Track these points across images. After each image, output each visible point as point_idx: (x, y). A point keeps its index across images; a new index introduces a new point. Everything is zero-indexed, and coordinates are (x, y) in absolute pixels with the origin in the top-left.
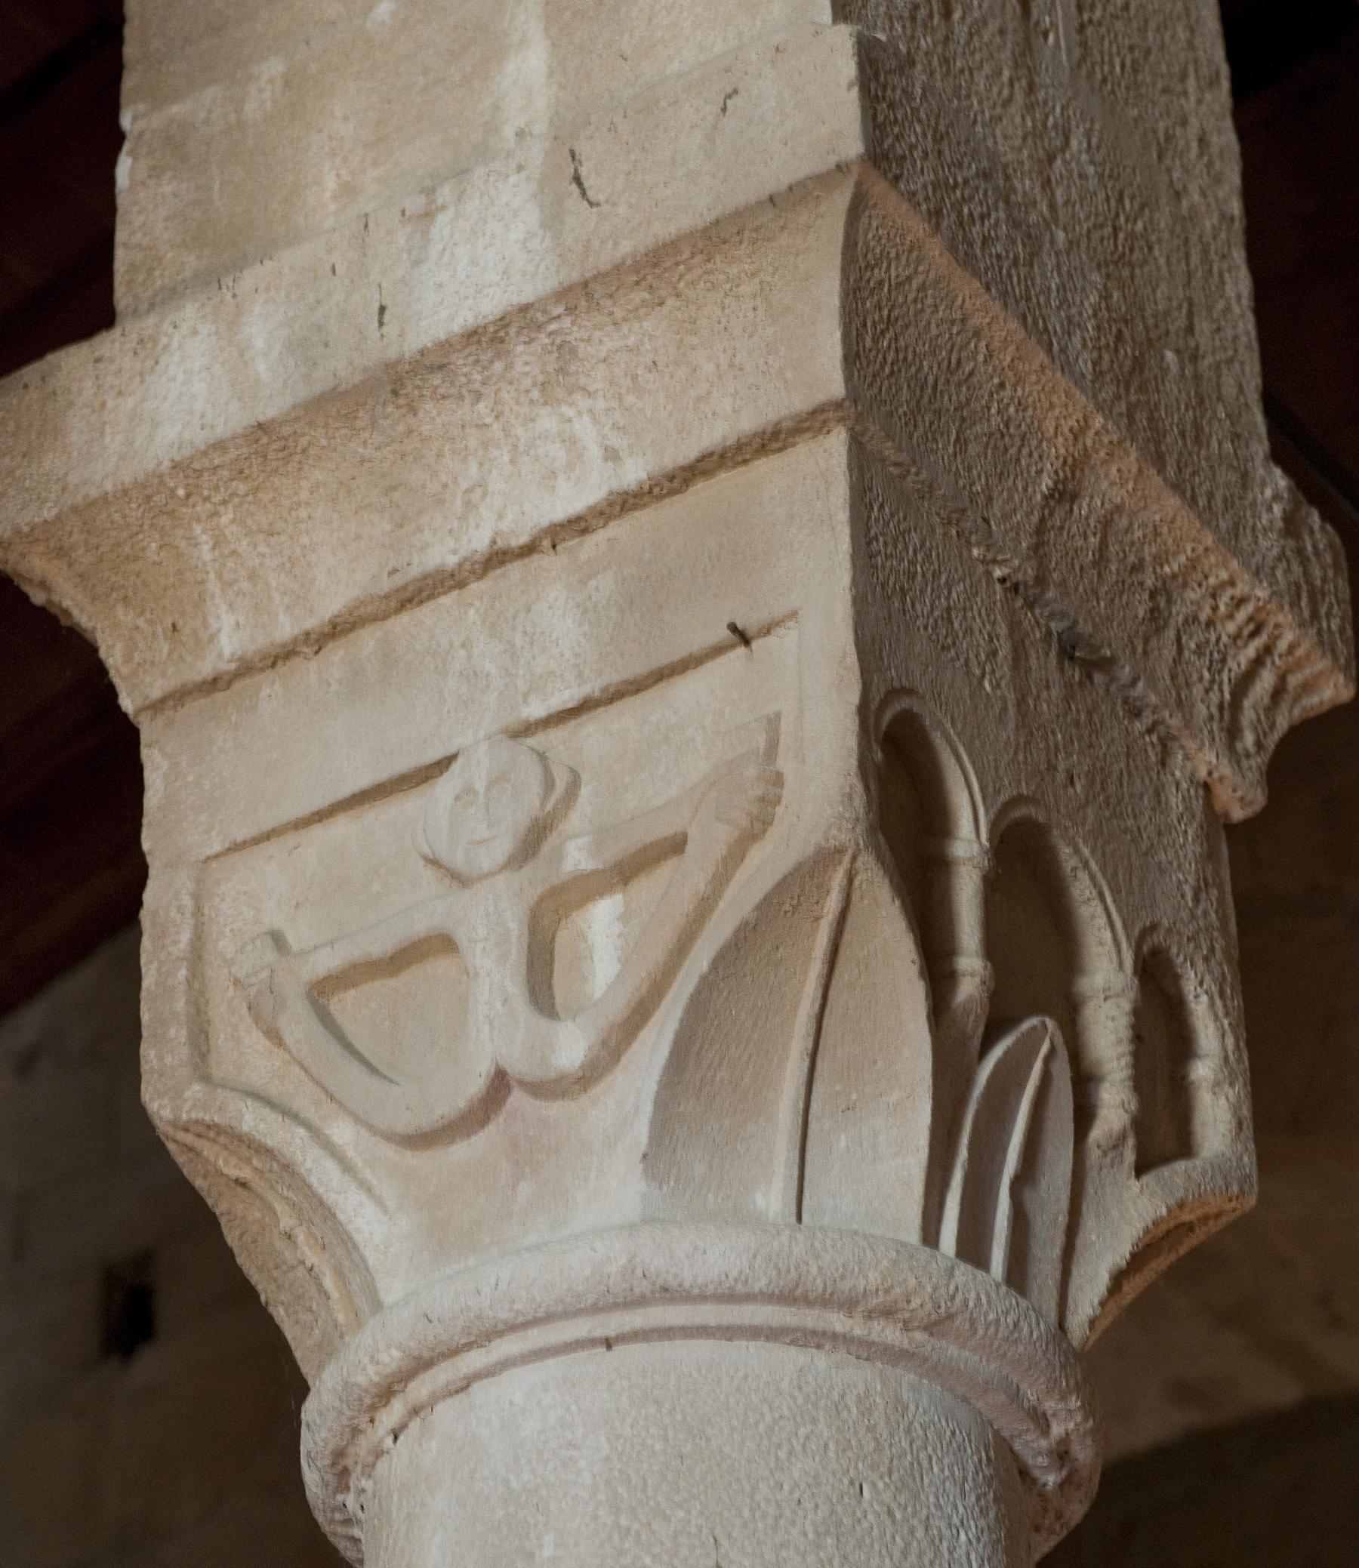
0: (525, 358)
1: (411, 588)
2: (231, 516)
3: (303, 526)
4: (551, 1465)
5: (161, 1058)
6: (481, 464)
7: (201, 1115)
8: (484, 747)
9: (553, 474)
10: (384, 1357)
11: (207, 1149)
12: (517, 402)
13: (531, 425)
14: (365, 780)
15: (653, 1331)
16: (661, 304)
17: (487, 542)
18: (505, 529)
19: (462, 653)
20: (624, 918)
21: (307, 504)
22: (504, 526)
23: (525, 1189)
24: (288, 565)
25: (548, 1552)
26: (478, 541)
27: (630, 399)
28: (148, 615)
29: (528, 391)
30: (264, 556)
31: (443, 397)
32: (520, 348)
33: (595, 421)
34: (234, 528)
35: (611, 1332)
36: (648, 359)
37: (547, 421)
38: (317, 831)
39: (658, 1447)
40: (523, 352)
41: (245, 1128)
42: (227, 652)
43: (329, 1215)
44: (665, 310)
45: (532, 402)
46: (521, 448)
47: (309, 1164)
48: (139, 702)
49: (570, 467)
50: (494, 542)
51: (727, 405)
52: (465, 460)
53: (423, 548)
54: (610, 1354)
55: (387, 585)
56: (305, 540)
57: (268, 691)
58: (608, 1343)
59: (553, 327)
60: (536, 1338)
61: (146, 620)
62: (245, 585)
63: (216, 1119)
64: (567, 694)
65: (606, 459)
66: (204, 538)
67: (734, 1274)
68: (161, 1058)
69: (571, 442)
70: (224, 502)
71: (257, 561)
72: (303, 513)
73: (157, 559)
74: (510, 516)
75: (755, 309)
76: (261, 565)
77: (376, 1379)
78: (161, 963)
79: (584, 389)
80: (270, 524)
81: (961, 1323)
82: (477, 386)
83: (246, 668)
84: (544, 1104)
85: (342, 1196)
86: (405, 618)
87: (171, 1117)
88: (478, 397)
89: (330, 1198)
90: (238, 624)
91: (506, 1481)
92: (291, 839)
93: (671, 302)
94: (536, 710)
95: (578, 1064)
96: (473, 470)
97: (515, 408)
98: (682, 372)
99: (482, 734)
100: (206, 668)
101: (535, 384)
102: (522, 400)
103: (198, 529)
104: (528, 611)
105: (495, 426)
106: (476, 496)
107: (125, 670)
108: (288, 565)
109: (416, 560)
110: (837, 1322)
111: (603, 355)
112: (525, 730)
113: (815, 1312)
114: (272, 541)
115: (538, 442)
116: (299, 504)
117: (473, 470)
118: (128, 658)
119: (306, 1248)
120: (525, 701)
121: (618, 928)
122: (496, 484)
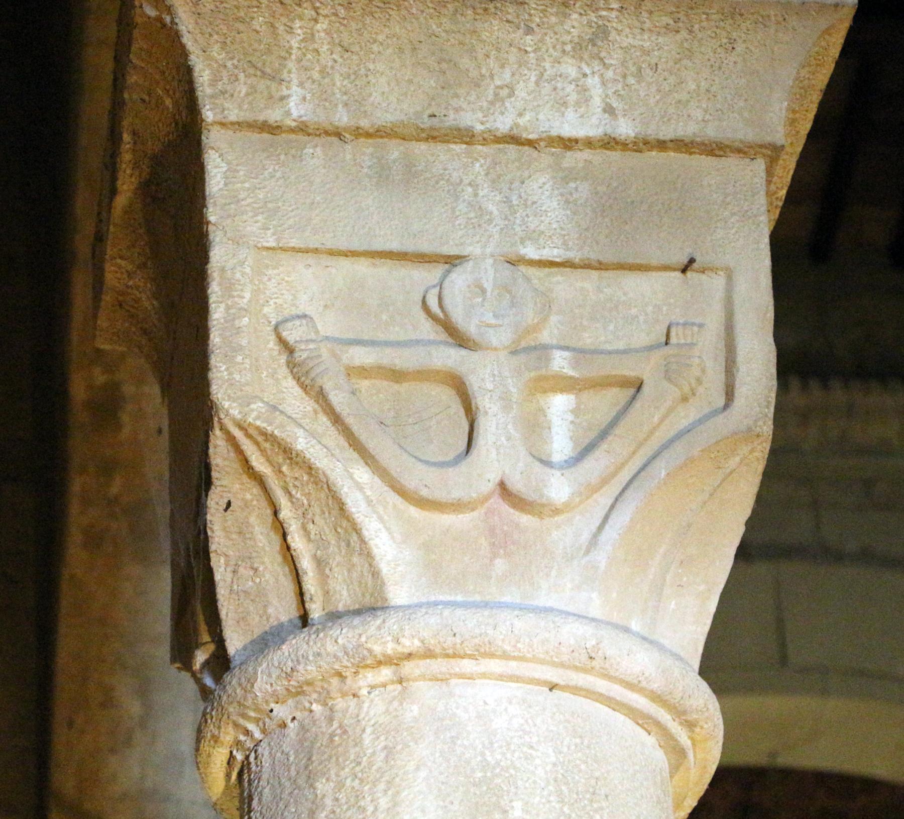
0: (576, 24)
1: (443, 131)
2: (325, 26)
3: (372, 56)
4: (517, 754)
6: (513, 75)
9: (565, 104)
10: (406, 642)
12: (554, 47)
13: (556, 65)
14: (394, 245)
15: (581, 689)
16: (678, 32)
17: (508, 127)
18: (521, 124)
19: (470, 189)
21: (381, 44)
22: (521, 121)
24: (353, 77)
25: (518, 813)
26: (503, 123)
27: (631, 80)
28: (235, 62)
29: (564, 43)
30: (335, 61)
31: (508, 21)
32: (575, 16)
33: (603, 83)
34: (323, 34)
35: (555, 680)
36: (653, 61)
37: (570, 69)
39: (583, 767)
40: (576, 19)
42: (295, 114)
43: (356, 529)
44: (678, 37)
45: (564, 51)
46: (546, 77)
47: (346, 489)
48: (219, 118)
49: (578, 104)
50: (511, 129)
51: (698, 114)
52: (502, 66)
53: (457, 110)
55: (426, 123)
56: (371, 66)
57: (311, 151)
59: (604, 13)
60: (513, 667)
61: (233, 64)
62: (316, 76)
63: (276, 432)
65: (605, 111)
66: (299, 31)
67: (647, 674)
69: (583, 90)
70: (326, 16)
71: (330, 64)
72: (375, 48)
73: (258, 28)
74: (527, 117)
75: (735, 63)
76: (332, 67)
78: (228, 308)
79: (601, 59)
80: (350, 44)
82: (533, 25)
83: (302, 129)
84: (517, 513)
86: (423, 146)
87: (239, 417)
88: (529, 31)
89: (359, 517)
90: (304, 99)
91: (483, 754)
92: (326, 260)
93: (684, 34)
94: (531, 252)
95: (563, 500)
96: (507, 75)
97: (551, 50)
98: (672, 80)
99: (488, 251)
100: (274, 116)
101: (571, 42)
102: (558, 47)
103: (298, 24)
104: (523, 183)
105: (532, 55)
106: (504, 92)
107: (209, 91)
108: (353, 77)
109: (452, 116)
110: (665, 717)
111: (625, 45)
112: (515, 262)
114: (346, 55)
115: (559, 79)
116: (375, 41)
117: (507, 75)
118: (213, 82)
119: (296, 535)
122: (521, 91)
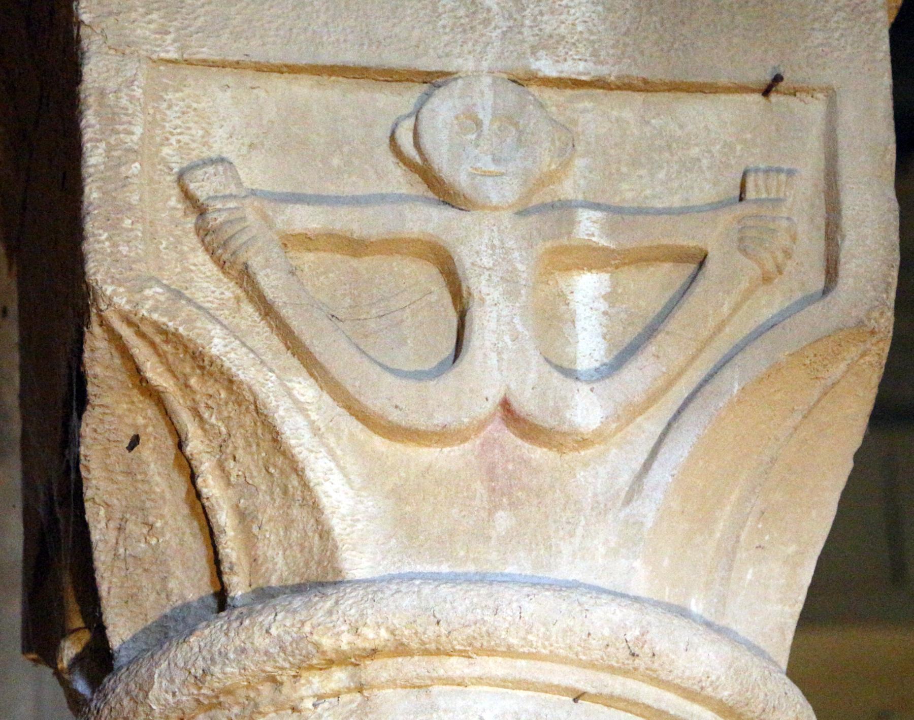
5: (115, 245)
7: (164, 320)
8: (487, 80)
11: (96, 329)
15: (620, 699)
20: (611, 297)
23: (503, 520)
38: (279, 82)
41: (214, 351)
43: (296, 468)
47: (281, 412)
54: (575, 705)
58: (578, 697)
60: (522, 668)
63: (181, 330)
64: (581, 66)
68: (115, 245)
77: (345, 647)
78: (110, 148)
81: (110, 509)
84: (527, 445)
85: (313, 455)
99: (485, 65)
113: (620, 679)
120: (533, 53)
121: (603, 306)
